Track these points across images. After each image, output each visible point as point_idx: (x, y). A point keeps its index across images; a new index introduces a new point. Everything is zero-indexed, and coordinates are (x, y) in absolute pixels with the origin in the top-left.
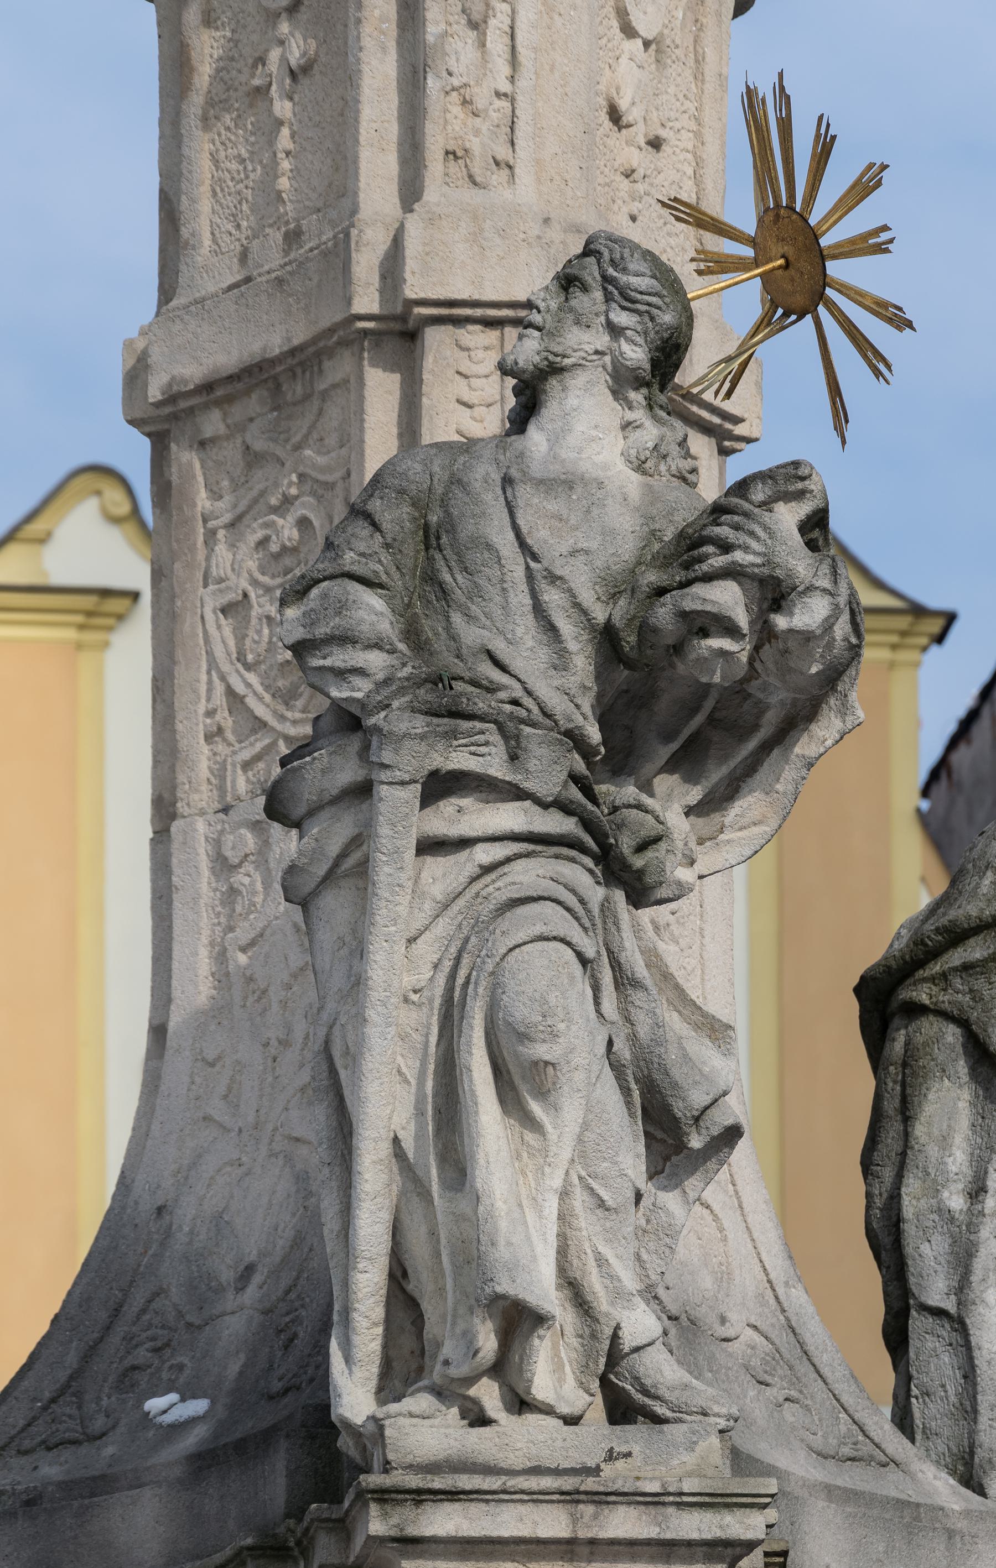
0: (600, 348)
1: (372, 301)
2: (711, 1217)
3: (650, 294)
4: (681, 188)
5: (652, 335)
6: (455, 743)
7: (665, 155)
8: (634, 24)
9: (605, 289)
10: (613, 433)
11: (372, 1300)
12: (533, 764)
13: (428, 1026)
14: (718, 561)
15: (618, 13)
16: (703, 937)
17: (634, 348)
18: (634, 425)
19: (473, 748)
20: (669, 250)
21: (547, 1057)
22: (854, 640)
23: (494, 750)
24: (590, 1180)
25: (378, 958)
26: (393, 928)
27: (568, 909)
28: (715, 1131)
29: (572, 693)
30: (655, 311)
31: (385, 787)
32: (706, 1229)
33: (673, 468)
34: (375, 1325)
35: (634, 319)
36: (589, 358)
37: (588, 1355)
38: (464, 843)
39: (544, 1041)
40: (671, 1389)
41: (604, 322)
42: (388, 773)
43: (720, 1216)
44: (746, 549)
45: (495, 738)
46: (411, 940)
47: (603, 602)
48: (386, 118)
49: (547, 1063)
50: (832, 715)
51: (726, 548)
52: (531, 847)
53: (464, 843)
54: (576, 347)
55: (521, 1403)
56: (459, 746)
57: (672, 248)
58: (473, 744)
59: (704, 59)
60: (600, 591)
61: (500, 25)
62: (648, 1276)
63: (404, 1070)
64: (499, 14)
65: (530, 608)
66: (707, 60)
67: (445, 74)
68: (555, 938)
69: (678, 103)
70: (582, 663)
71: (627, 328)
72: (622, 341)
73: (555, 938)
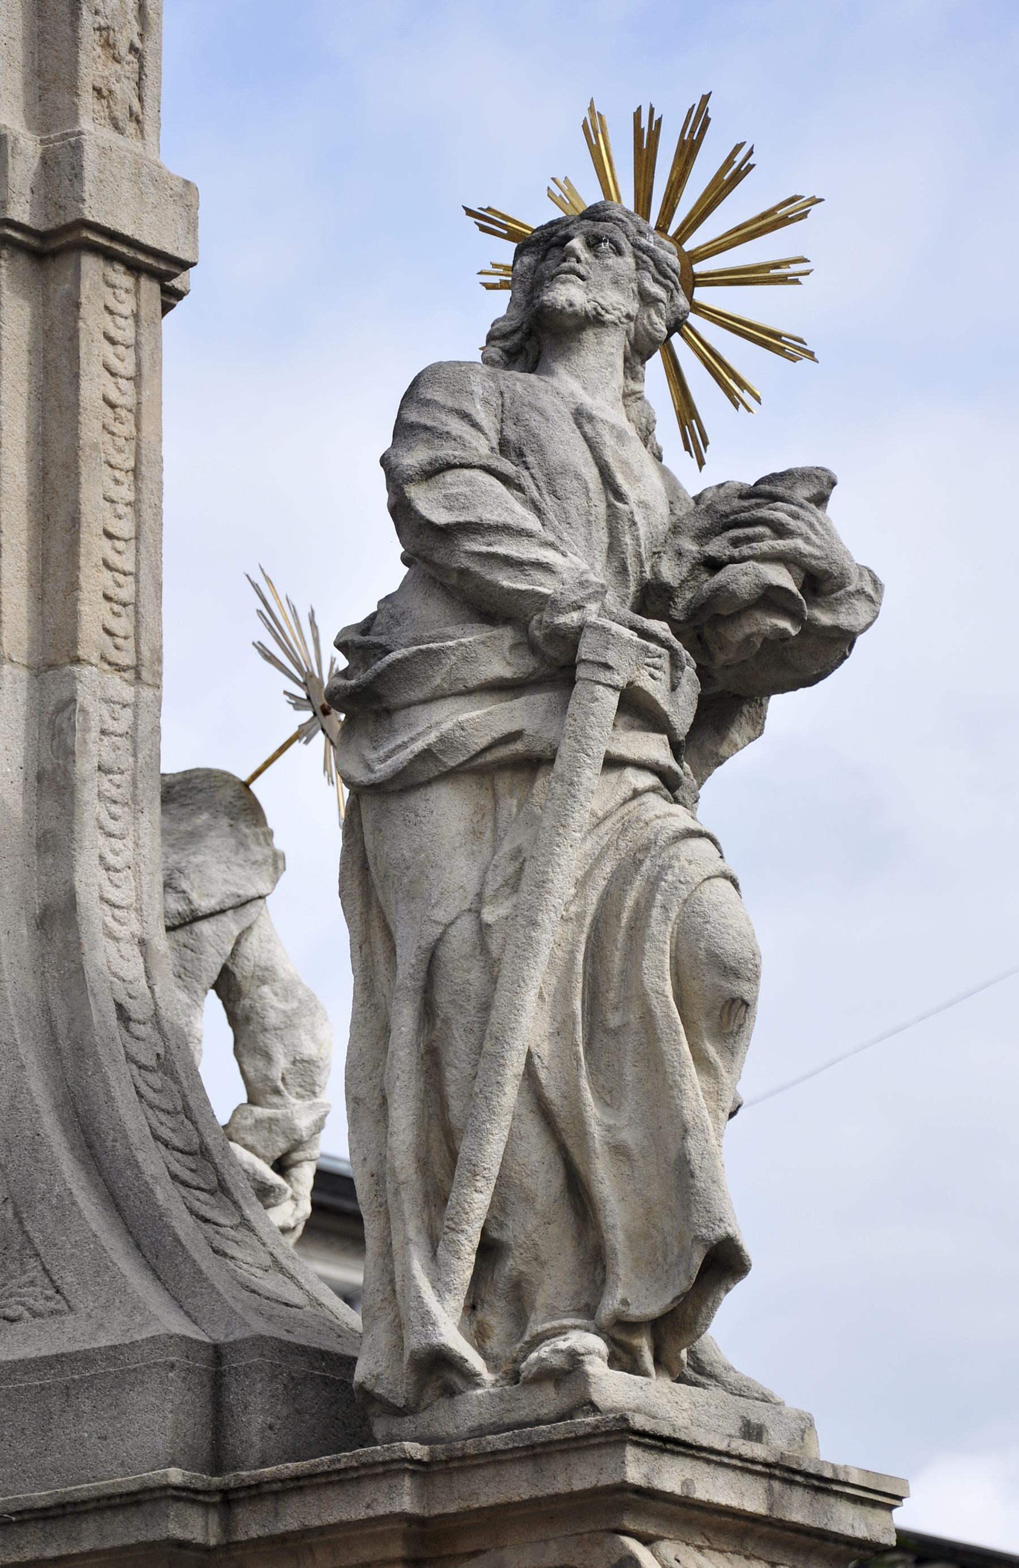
1: (24, 212)
9: (636, 257)
13: (575, 943)
14: (771, 544)
30: (675, 292)
41: (636, 289)
42: (608, 674)
44: (807, 540)
45: (665, 663)
50: (743, 721)
51: (780, 531)
65: (606, 545)
72: (652, 312)
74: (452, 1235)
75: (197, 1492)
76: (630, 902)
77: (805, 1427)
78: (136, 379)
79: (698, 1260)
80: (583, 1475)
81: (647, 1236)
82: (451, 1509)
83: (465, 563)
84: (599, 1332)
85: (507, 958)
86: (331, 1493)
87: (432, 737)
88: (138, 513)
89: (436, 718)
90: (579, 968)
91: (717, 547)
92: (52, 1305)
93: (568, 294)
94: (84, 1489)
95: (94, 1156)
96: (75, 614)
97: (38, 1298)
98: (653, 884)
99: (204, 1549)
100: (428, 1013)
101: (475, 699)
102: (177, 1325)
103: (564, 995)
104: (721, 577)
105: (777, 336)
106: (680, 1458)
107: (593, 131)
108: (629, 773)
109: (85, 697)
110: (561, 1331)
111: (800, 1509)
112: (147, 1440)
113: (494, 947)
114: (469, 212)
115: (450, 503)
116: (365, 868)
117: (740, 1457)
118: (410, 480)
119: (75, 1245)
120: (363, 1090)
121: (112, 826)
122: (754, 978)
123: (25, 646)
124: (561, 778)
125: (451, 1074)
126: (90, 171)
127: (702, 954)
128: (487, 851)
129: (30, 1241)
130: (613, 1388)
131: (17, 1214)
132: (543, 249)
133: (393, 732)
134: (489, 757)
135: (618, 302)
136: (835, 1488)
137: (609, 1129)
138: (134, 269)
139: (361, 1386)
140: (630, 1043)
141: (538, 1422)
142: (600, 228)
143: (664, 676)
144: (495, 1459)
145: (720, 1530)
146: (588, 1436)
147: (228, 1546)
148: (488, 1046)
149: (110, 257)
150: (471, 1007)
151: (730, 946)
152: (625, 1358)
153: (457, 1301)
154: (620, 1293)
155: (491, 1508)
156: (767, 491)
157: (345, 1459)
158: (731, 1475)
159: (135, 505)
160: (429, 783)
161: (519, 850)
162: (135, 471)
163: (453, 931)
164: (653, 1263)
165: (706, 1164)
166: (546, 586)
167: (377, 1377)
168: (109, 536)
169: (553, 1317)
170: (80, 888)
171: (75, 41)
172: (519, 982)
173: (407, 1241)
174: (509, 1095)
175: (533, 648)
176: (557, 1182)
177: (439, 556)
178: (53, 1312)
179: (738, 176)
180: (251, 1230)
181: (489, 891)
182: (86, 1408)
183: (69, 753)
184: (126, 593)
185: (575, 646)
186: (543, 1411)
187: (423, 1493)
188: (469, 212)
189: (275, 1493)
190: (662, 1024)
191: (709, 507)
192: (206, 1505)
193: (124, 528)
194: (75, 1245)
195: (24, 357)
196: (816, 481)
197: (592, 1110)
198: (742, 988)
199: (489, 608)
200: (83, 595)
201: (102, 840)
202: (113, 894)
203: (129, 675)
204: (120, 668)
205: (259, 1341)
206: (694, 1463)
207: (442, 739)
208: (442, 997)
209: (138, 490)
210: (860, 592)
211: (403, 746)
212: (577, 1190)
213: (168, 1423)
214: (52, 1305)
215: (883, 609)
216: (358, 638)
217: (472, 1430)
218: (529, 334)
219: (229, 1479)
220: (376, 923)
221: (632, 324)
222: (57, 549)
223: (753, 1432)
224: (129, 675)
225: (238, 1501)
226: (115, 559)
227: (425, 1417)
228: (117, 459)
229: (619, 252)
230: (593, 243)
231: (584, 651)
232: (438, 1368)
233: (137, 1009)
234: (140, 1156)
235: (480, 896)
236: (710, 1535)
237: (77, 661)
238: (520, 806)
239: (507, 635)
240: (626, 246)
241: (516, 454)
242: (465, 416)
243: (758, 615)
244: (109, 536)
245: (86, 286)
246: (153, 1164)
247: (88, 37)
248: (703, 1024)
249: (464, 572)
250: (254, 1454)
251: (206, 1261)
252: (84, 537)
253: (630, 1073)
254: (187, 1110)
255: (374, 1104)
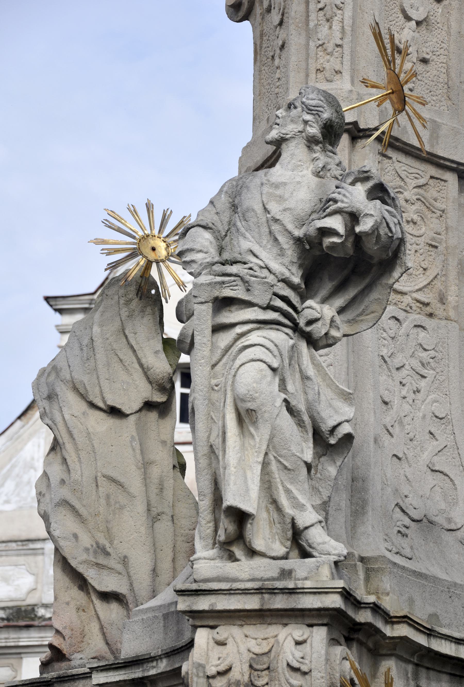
0: (300, 130)
2: (449, 480)
3: (317, 107)
4: (440, 77)
5: (320, 123)
6: (224, 286)
7: (431, 65)
8: (409, 15)
10: (309, 163)
11: (206, 512)
12: (256, 293)
15: (402, 11)
16: (449, 367)
17: (312, 128)
18: (316, 159)
19: (231, 288)
20: (432, 101)
21: (251, 408)
22: (390, 235)
23: (240, 288)
24: (279, 458)
25: (198, 373)
26: (203, 361)
27: (267, 349)
28: (340, 436)
29: (286, 264)
30: (320, 113)
31: (196, 305)
32: (446, 485)
33: (333, 174)
34: (209, 522)
35: (311, 117)
36: (296, 134)
37: (284, 531)
38: (233, 325)
39: (249, 401)
40: (319, 544)
43: (453, 479)
44: (342, 202)
45: (240, 283)
46: (214, 366)
47: (298, 228)
48: (300, 60)
49: (252, 410)
52: (258, 326)
53: (233, 325)
54: (291, 130)
55: (252, 553)
56: (226, 287)
57: (434, 100)
58: (231, 286)
59: (451, 26)
60: (297, 224)
61: (339, 19)
62: (323, 498)
63: (214, 417)
64: (338, 15)
66: (452, 27)
67: (316, 40)
68: (258, 360)
69: (438, 45)
70: (291, 253)
71: (309, 121)
73: (258, 360)
106: (209, 596)
136: (298, 591)
158: (239, 596)
196: (353, 174)
206: (217, 596)
221: (303, 134)
236: (245, 619)
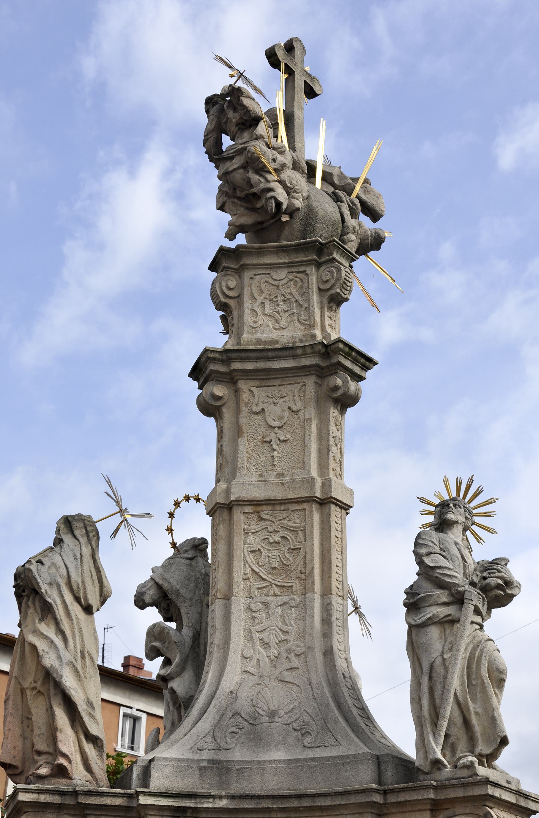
13: (464, 664)
14: (497, 574)
44: (505, 574)
45: (481, 600)
51: (499, 571)
74: (439, 732)
75: (378, 790)
76: (477, 655)
77: (518, 783)
78: (341, 532)
79: (499, 741)
80: (477, 791)
81: (484, 734)
82: (443, 798)
83: (437, 575)
84: (475, 757)
85: (450, 666)
86: (412, 792)
87: (431, 614)
88: (342, 561)
89: (431, 610)
90: (466, 670)
91: (485, 574)
92: (336, 743)
93: (450, 516)
94: (351, 788)
95: (340, 709)
96: (331, 583)
97: (332, 741)
98: (482, 651)
99: (380, 804)
100: (430, 678)
101: (439, 606)
102: (366, 750)
103: (462, 676)
104: (487, 581)
105: (489, 528)
107: (446, 482)
108: (474, 625)
109: (333, 603)
110: (466, 756)
111: (522, 803)
112: (364, 777)
113: (447, 664)
114: (418, 498)
115: (433, 561)
116: (413, 644)
117: (510, 789)
118: (423, 556)
119: (340, 730)
120: (414, 696)
121: (339, 632)
122: (506, 675)
123: (319, 590)
124: (461, 625)
125: (436, 693)
126: (333, 486)
127: (495, 668)
128: (443, 642)
129: (328, 728)
130: (482, 771)
131: (325, 722)
132: (444, 506)
133: (420, 613)
134: (444, 620)
135: (461, 519)
137: (475, 708)
138: (341, 507)
139: (417, 767)
140: (479, 688)
141: (463, 778)
142: (456, 502)
143: (481, 603)
144: (454, 786)
145: (505, 806)
146: (478, 782)
147: (385, 804)
148: (446, 687)
149: (336, 505)
150: (441, 678)
151: (501, 666)
152: (481, 763)
153: (440, 748)
154: (480, 748)
155: (452, 798)
156: (495, 562)
157: (410, 784)
159: (342, 559)
160: (430, 625)
161: (452, 642)
162: (342, 552)
163: (436, 660)
164: (488, 741)
165: (499, 718)
166: (456, 581)
167: (421, 765)
168: (337, 566)
169: (462, 753)
170: (334, 646)
171: (329, 459)
172: (453, 672)
173: (428, 733)
174: (451, 699)
175: (452, 595)
176: (462, 720)
177: (431, 573)
178: (336, 745)
179: (480, 493)
180: (376, 728)
181: (445, 651)
182: (348, 768)
183: (330, 615)
184: (340, 579)
185: (463, 595)
186: (464, 775)
187: (435, 794)
188: (418, 498)
189: (397, 792)
190: (486, 684)
191: (482, 565)
192: (380, 793)
193: (340, 565)
194: (340, 730)
195: (318, 526)
197: (471, 704)
198: (503, 676)
199: (442, 585)
200: (332, 579)
201: (337, 635)
202: (340, 648)
203: (341, 598)
204: (340, 596)
205: (388, 755)
207: (433, 615)
208: (434, 675)
209: (342, 556)
210: (517, 586)
211: (424, 616)
212: (467, 723)
213: (369, 773)
214: (336, 743)
215: (521, 590)
216: (409, 591)
217: (445, 779)
218: (440, 525)
219: (385, 787)
220: (415, 657)
222: (326, 569)
223: (509, 782)
224: (341, 598)
225: (388, 793)
226: (338, 572)
227: (433, 775)
228: (338, 549)
229: (460, 508)
230: (455, 505)
231: (466, 596)
232: (437, 763)
233: (347, 675)
234: (352, 709)
235: (443, 652)
237: (331, 594)
238: (450, 632)
239: (446, 592)
240: (462, 506)
241: (444, 551)
242: (433, 542)
243: (496, 590)
244: (337, 566)
245: (332, 511)
246: (355, 711)
247: (331, 458)
248: (495, 684)
249: (437, 577)
250: (389, 782)
251: (370, 735)
252: (332, 566)
253: (479, 695)
254: (359, 699)
255: (417, 700)
